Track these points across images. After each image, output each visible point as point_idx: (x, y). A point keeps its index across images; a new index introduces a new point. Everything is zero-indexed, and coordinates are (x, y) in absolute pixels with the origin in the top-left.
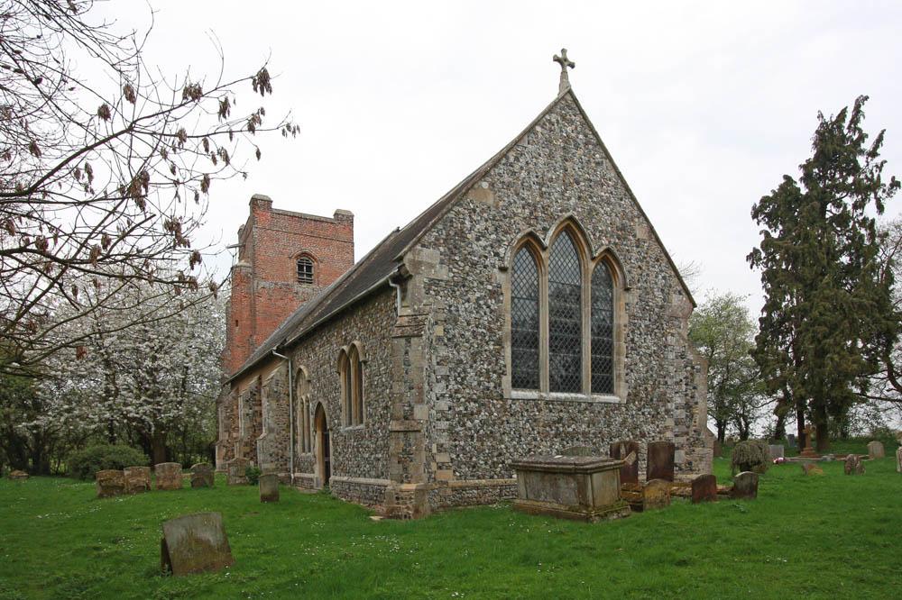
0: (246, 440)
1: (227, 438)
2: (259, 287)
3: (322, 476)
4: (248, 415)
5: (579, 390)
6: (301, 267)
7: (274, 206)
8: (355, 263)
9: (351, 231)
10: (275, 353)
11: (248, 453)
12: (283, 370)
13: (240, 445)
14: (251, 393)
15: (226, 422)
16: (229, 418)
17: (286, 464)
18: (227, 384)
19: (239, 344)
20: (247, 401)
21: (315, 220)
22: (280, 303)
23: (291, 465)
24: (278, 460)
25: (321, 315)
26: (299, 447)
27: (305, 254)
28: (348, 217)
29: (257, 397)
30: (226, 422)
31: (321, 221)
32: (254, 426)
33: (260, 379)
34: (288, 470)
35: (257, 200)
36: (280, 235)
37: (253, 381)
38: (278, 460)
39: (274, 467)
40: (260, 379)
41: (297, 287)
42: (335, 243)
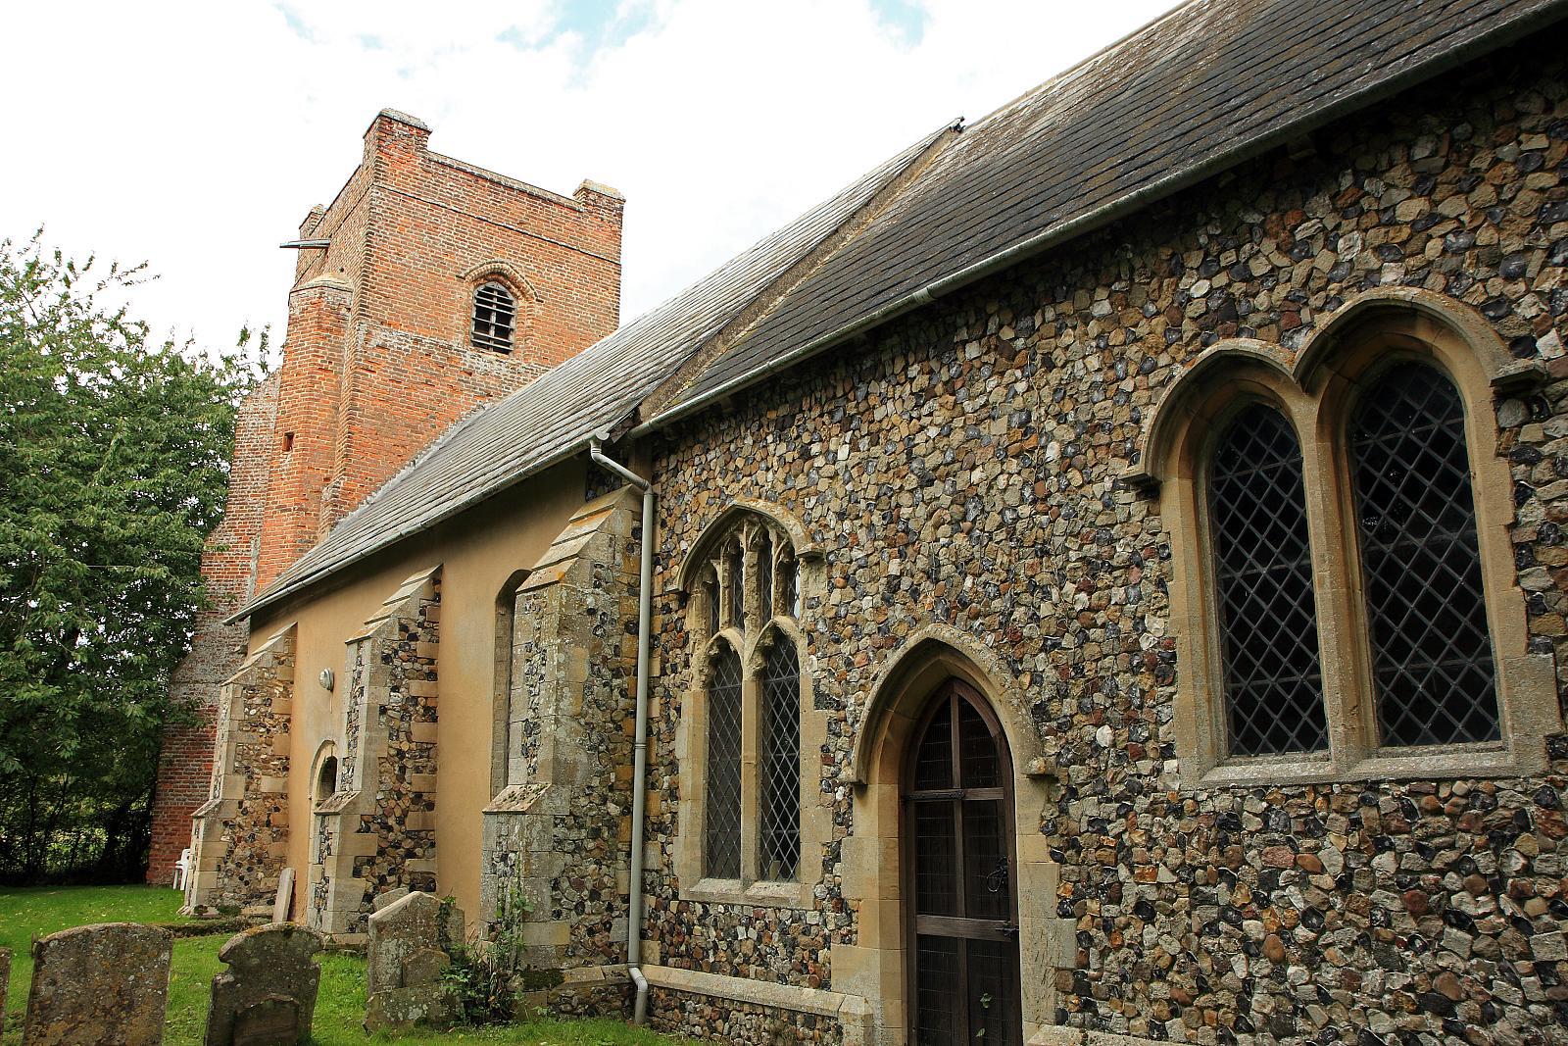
0: (367, 808)
1: (239, 794)
2: (373, 343)
3: (896, 1009)
4: (383, 710)
5: (1312, 738)
6: (483, 313)
7: (433, 144)
8: (626, 317)
9: (616, 236)
10: (596, 453)
11: (371, 861)
12: (622, 526)
13: (344, 826)
14: (404, 628)
15: (243, 738)
16: (254, 725)
17: (607, 926)
18: (242, 618)
19: (290, 502)
20: (386, 659)
21: (530, 195)
22: (423, 394)
23: (624, 930)
24: (580, 907)
25: (733, 362)
26: (684, 850)
27: (497, 275)
28: (611, 200)
29: (421, 647)
30: (243, 738)
31: (544, 200)
32: (400, 754)
33: (436, 580)
34: (614, 954)
35: (391, 120)
36: (445, 220)
37: (411, 585)
38: (580, 907)
39: (565, 939)
40: (436, 580)
41: (470, 357)
42: (574, 257)
